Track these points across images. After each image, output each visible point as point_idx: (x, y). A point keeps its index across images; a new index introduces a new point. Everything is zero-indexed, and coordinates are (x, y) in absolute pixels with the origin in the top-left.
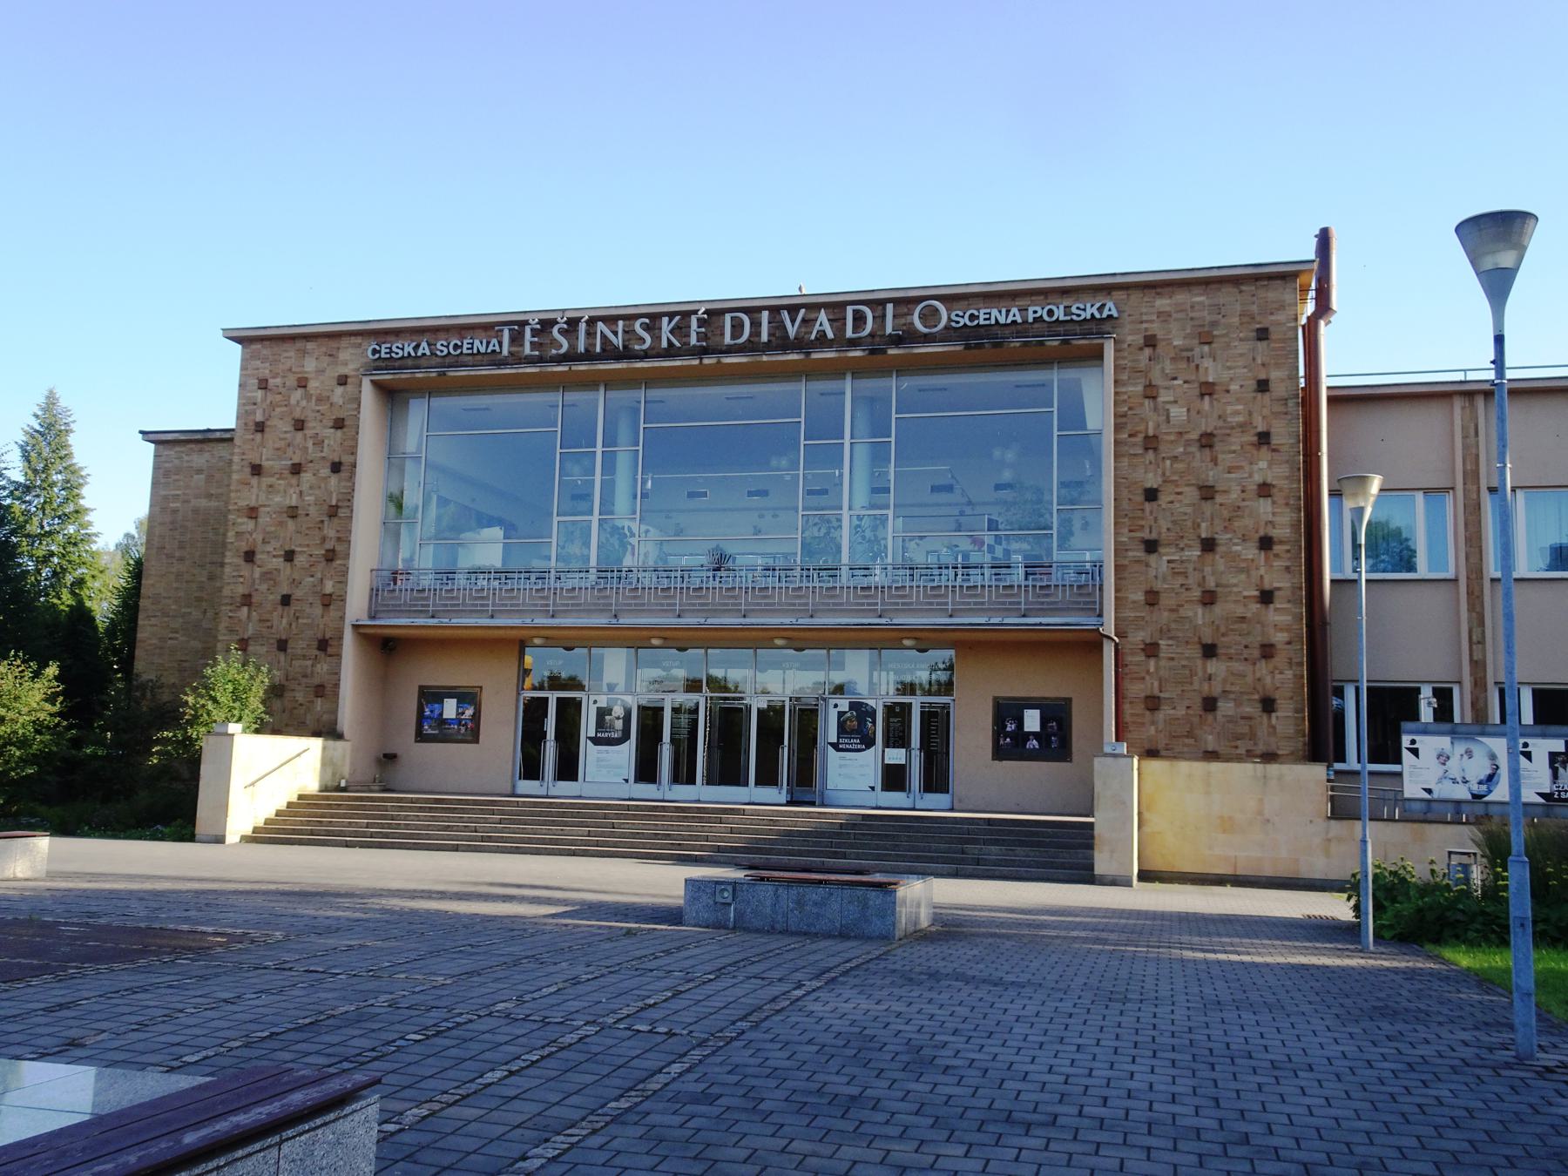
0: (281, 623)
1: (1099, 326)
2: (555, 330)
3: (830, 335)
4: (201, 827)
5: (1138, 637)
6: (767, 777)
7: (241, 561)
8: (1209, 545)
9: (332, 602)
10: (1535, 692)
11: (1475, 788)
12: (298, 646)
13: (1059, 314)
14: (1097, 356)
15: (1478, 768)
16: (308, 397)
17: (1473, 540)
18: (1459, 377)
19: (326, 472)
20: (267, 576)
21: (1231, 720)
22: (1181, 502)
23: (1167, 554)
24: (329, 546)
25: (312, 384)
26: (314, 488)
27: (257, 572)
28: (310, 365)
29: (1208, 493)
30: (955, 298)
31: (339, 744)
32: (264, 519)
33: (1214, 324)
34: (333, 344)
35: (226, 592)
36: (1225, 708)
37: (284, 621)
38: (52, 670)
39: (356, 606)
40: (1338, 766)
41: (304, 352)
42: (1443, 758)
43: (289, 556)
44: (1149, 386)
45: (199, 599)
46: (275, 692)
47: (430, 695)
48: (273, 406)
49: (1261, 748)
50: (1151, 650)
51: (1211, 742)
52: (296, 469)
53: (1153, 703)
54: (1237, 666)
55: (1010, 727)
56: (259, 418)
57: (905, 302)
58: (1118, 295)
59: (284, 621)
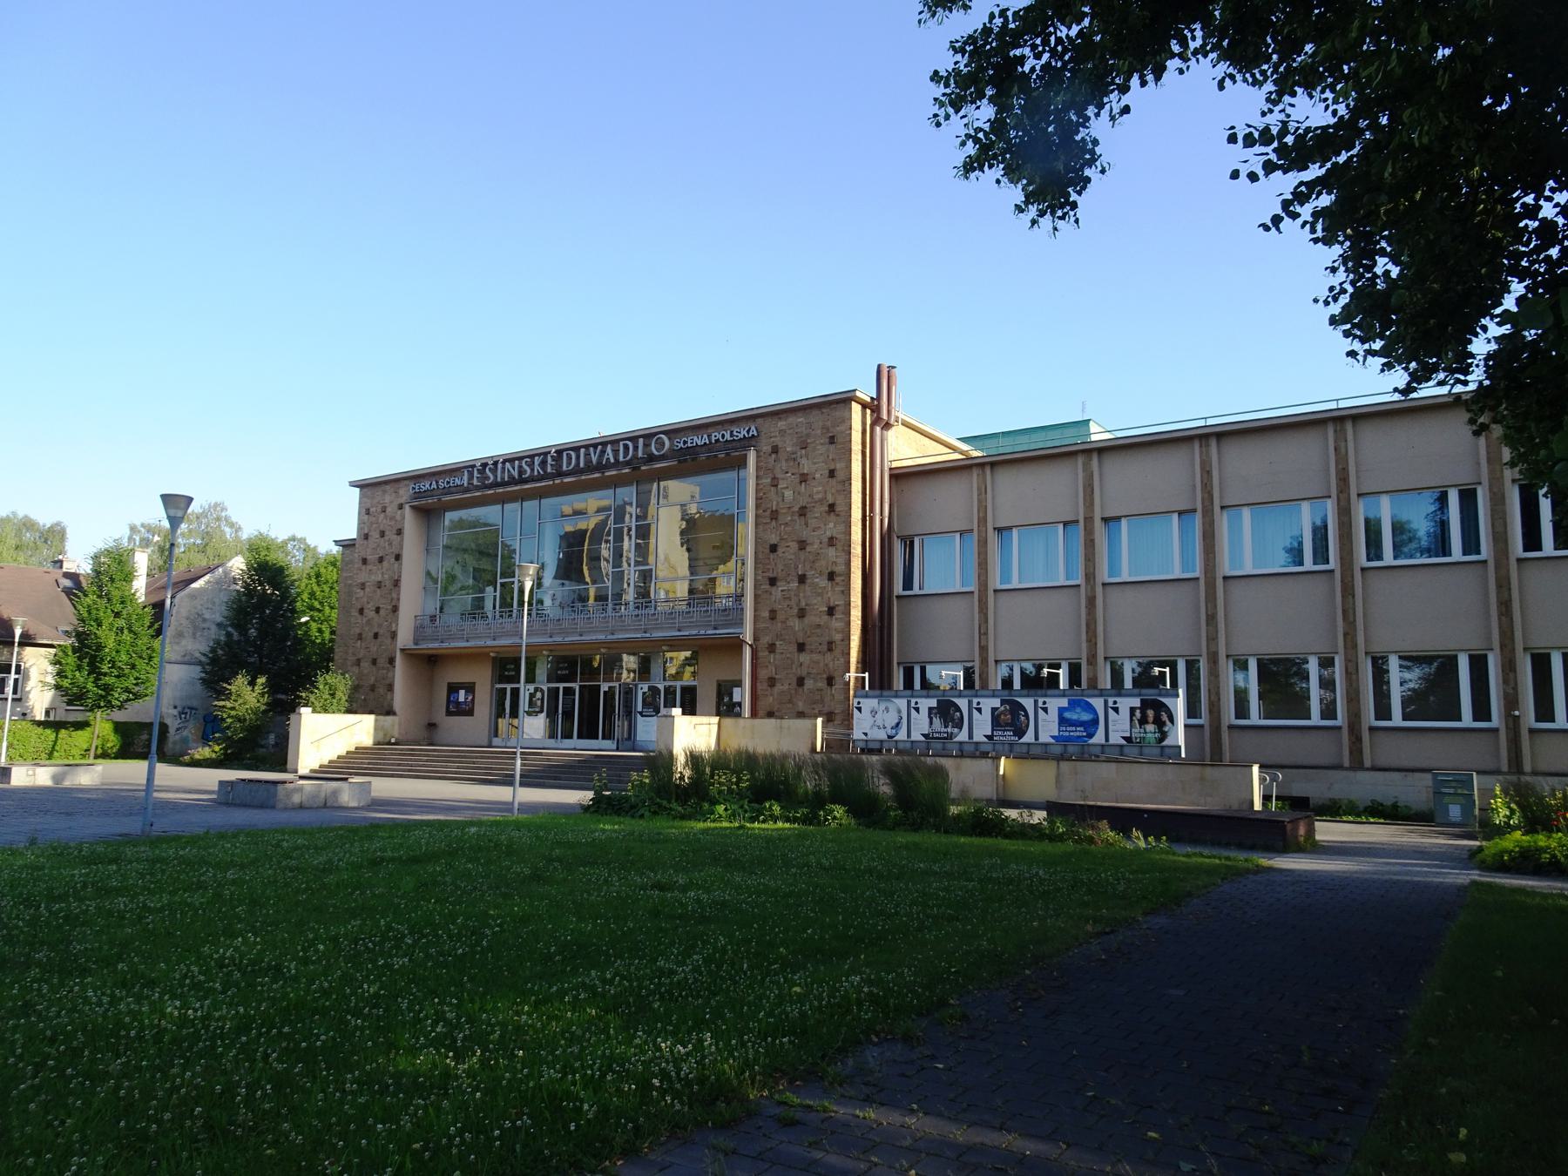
1: (748, 442)
4: (289, 766)
5: (765, 640)
6: (608, 735)
8: (802, 579)
9: (394, 635)
10: (1471, 657)
11: (890, 732)
13: (728, 437)
14: (741, 463)
15: (891, 719)
17: (983, 565)
18: (1333, 406)
21: (811, 691)
22: (789, 551)
23: (782, 586)
28: (387, 499)
29: (803, 545)
30: (673, 432)
31: (389, 718)
33: (808, 435)
36: (809, 684)
38: (261, 680)
39: (405, 637)
41: (384, 492)
42: (874, 713)
43: (378, 610)
44: (774, 478)
46: (356, 689)
47: (440, 691)
50: (772, 648)
51: (801, 706)
53: (772, 682)
54: (816, 657)
55: (726, 699)
57: (649, 436)
58: (760, 421)
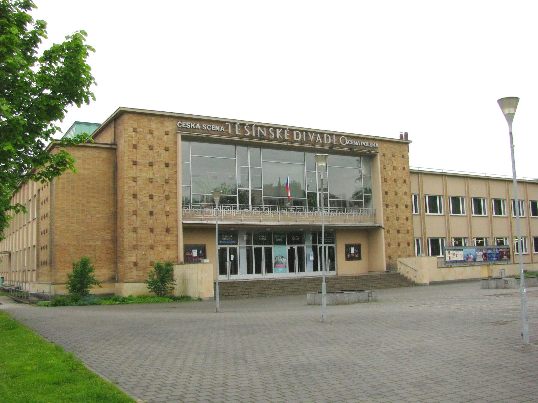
0: (150, 222)
2: (245, 127)
3: (321, 142)
7: (131, 198)
12: (157, 231)
13: (367, 145)
16: (154, 138)
18: (441, 171)
19: (163, 166)
20: (142, 204)
24: (166, 194)
25: (155, 133)
26: (159, 172)
27: (138, 202)
32: (139, 182)
34: (162, 119)
35: (126, 209)
36: (402, 244)
37: (151, 221)
40: (438, 256)
43: (151, 197)
45: (83, 210)
48: (139, 139)
49: (408, 254)
52: (151, 164)
56: (134, 143)
59: (151, 221)
